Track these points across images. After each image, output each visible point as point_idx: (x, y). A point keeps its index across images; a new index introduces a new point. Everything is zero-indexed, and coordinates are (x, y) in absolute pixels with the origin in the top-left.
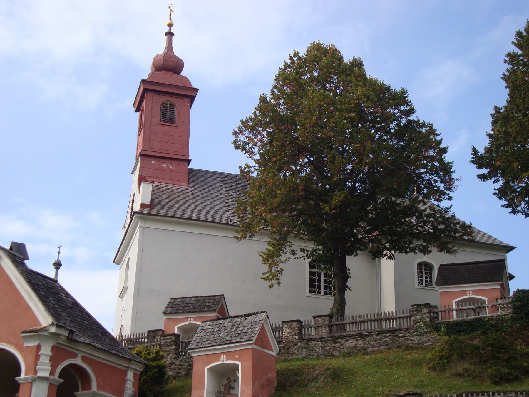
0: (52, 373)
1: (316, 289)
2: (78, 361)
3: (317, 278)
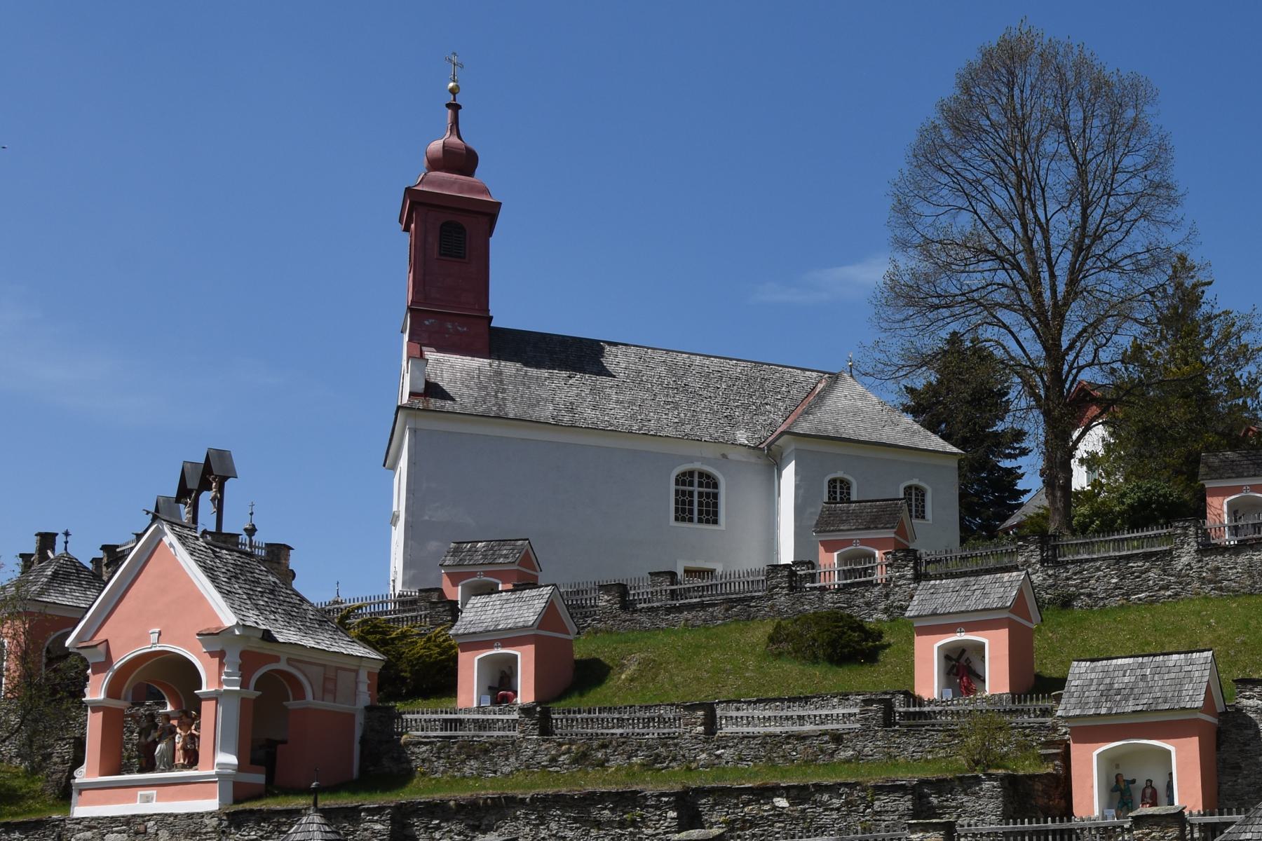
0: (244, 685)
1: (687, 515)
2: (282, 666)
3: (687, 498)
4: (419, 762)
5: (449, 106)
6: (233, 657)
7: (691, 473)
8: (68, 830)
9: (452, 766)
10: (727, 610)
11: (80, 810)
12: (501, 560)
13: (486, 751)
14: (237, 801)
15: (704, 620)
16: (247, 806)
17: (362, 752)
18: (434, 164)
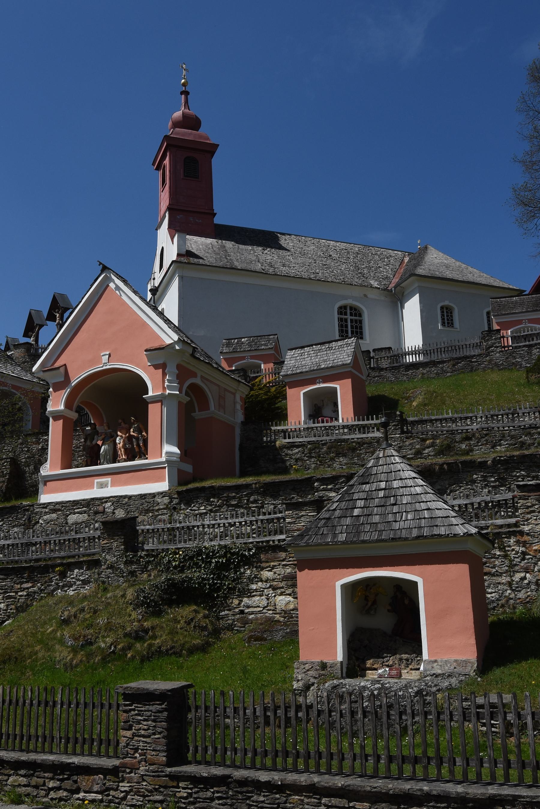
3: (344, 323)
4: (293, 462)
5: (182, 93)
6: (172, 368)
7: (345, 307)
8: (36, 513)
9: (322, 463)
10: (454, 365)
11: (45, 498)
12: (263, 347)
13: (354, 450)
14: (180, 484)
15: (437, 374)
16: (190, 486)
17: (241, 457)
18: (176, 124)
